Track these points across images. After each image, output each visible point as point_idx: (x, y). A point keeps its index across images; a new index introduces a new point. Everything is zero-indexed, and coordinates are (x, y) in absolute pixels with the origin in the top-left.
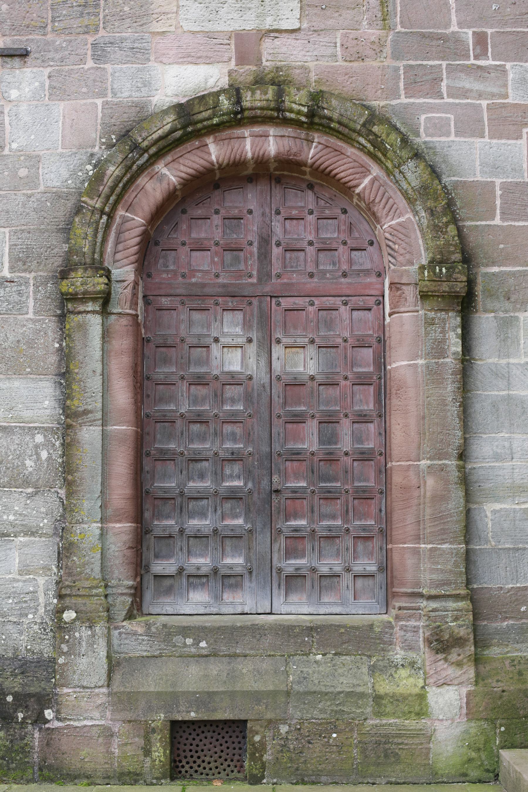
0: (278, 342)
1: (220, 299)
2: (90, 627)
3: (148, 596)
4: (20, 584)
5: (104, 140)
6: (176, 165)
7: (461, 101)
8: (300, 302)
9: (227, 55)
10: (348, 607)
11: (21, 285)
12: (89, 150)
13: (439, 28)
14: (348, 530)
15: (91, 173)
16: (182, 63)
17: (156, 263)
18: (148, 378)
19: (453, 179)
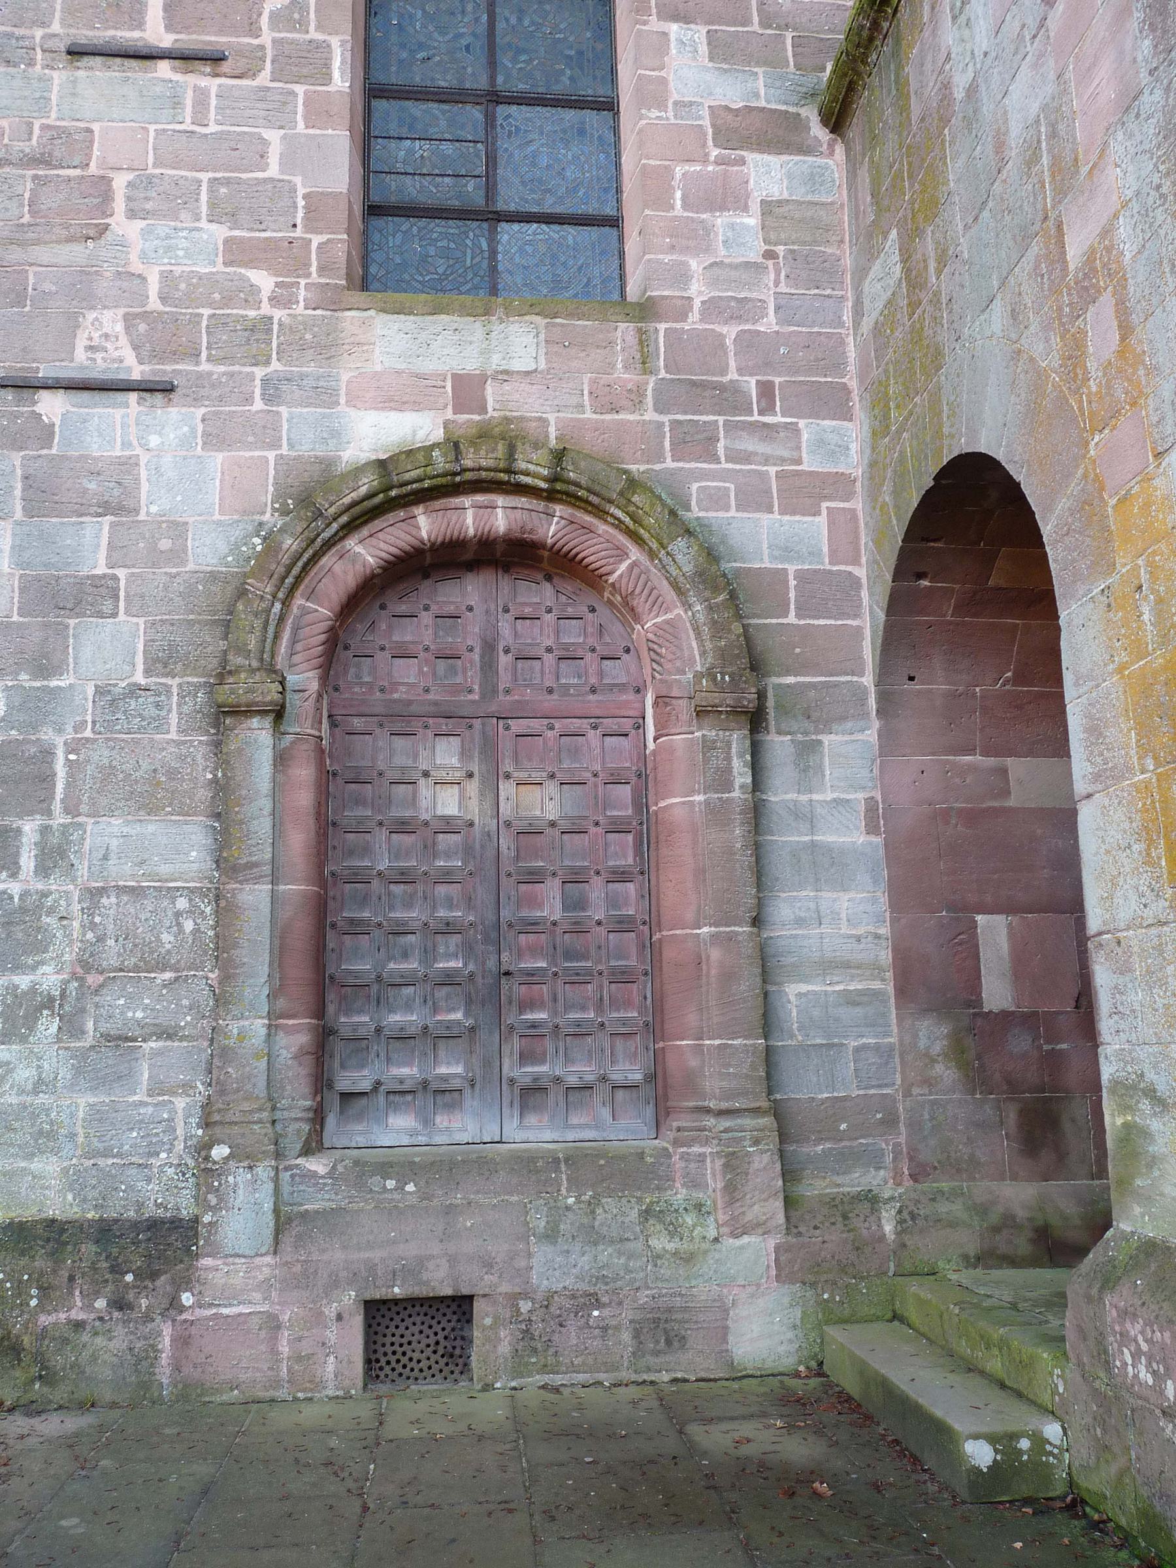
0: (508, 776)
1: (431, 721)
2: (250, 1168)
3: (331, 1121)
4: (150, 1109)
5: (277, 506)
6: (373, 541)
7: (743, 467)
8: (536, 725)
9: (441, 401)
10: (604, 1130)
11: (159, 695)
12: (257, 517)
13: (713, 375)
14: (602, 1025)
15: (259, 548)
16: (383, 409)
17: (346, 672)
18: (334, 824)
19: (734, 565)
